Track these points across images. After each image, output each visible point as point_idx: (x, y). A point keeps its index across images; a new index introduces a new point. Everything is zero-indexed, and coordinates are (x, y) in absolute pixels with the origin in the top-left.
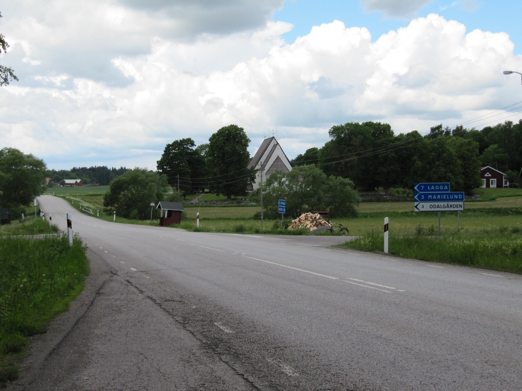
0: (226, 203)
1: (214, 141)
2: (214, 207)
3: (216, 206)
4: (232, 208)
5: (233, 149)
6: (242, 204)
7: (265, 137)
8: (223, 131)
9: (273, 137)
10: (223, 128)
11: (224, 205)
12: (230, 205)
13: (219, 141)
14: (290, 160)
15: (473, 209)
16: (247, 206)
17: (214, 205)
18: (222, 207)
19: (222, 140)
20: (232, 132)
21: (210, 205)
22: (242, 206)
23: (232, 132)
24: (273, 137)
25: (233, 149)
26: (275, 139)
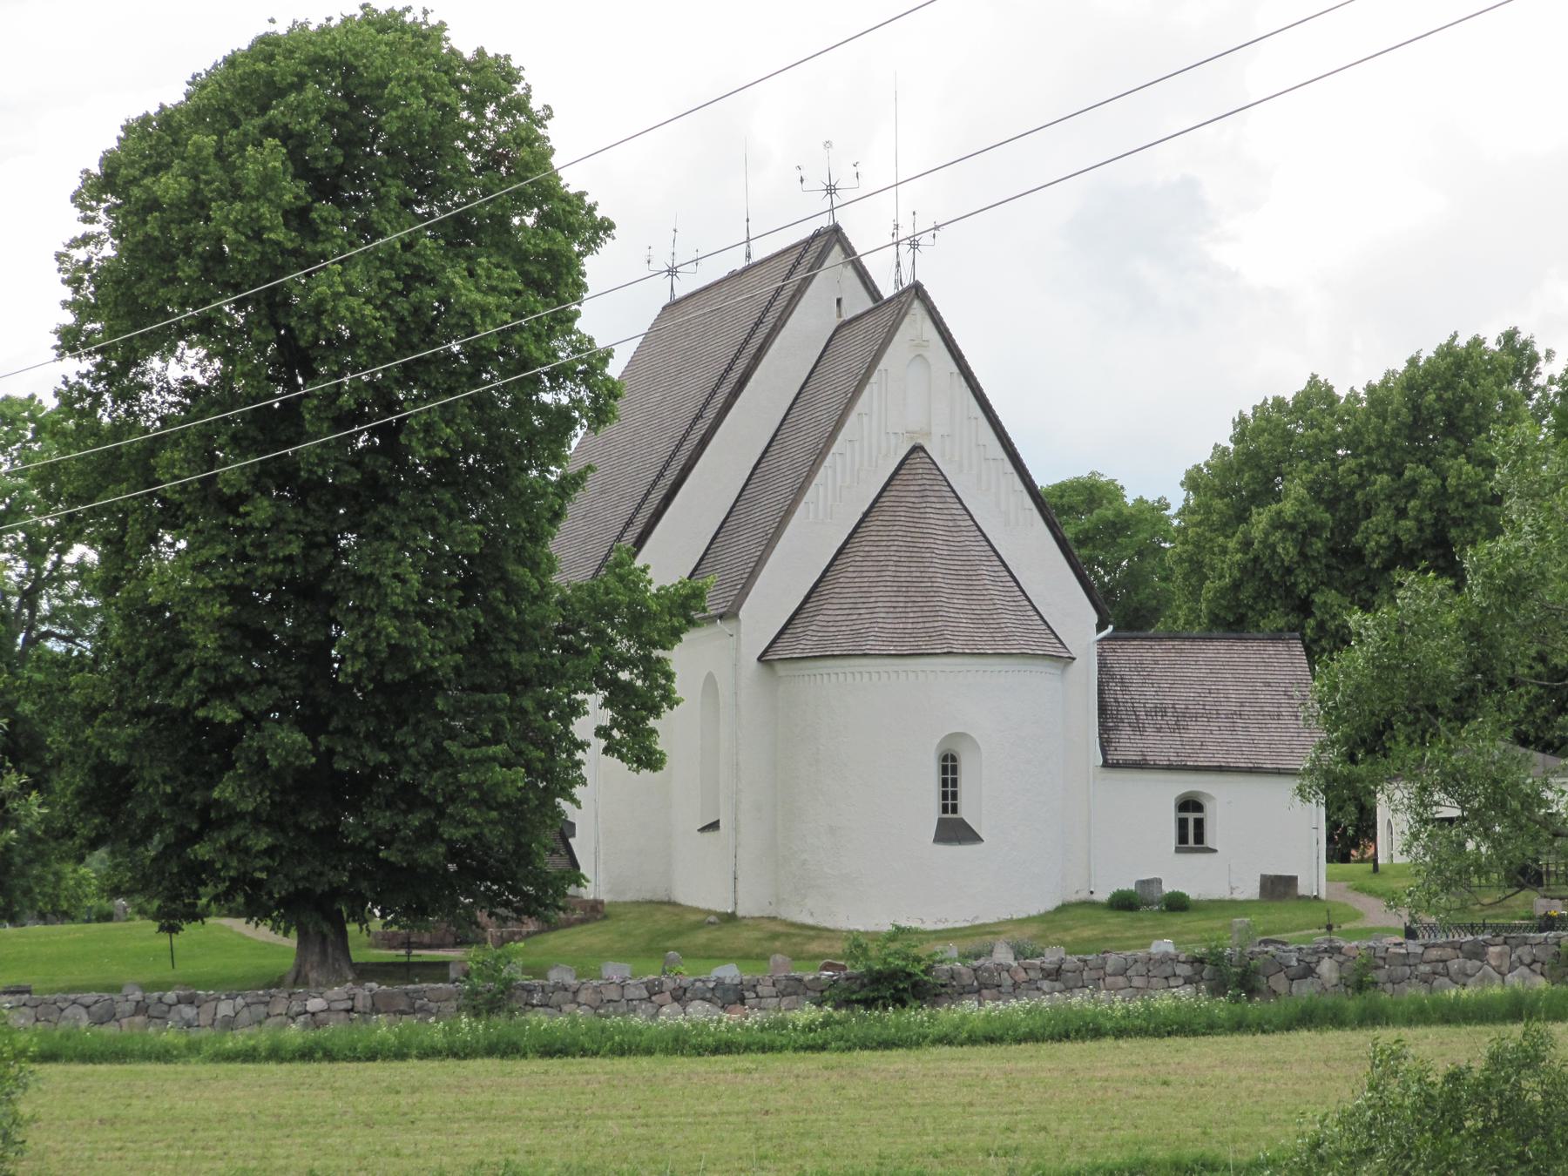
0: (315, 1004)
1: (170, 185)
2: (164, 1055)
3: (193, 1049)
4: (414, 1069)
5: (402, 306)
6: (540, 1020)
7: (672, 271)
8: (284, 68)
9: (833, 236)
10: (266, 47)
11: (294, 1034)
12: (384, 1029)
13: (234, 192)
14: (1042, 481)
15: (850, 932)
16: (621, 1051)
17: (170, 1036)
18: (276, 1054)
19: (268, 181)
20: (394, 89)
21: (109, 1030)
22: (552, 1049)
23: (394, 89)
24: (833, 236)
25: (402, 306)
26: (848, 250)
